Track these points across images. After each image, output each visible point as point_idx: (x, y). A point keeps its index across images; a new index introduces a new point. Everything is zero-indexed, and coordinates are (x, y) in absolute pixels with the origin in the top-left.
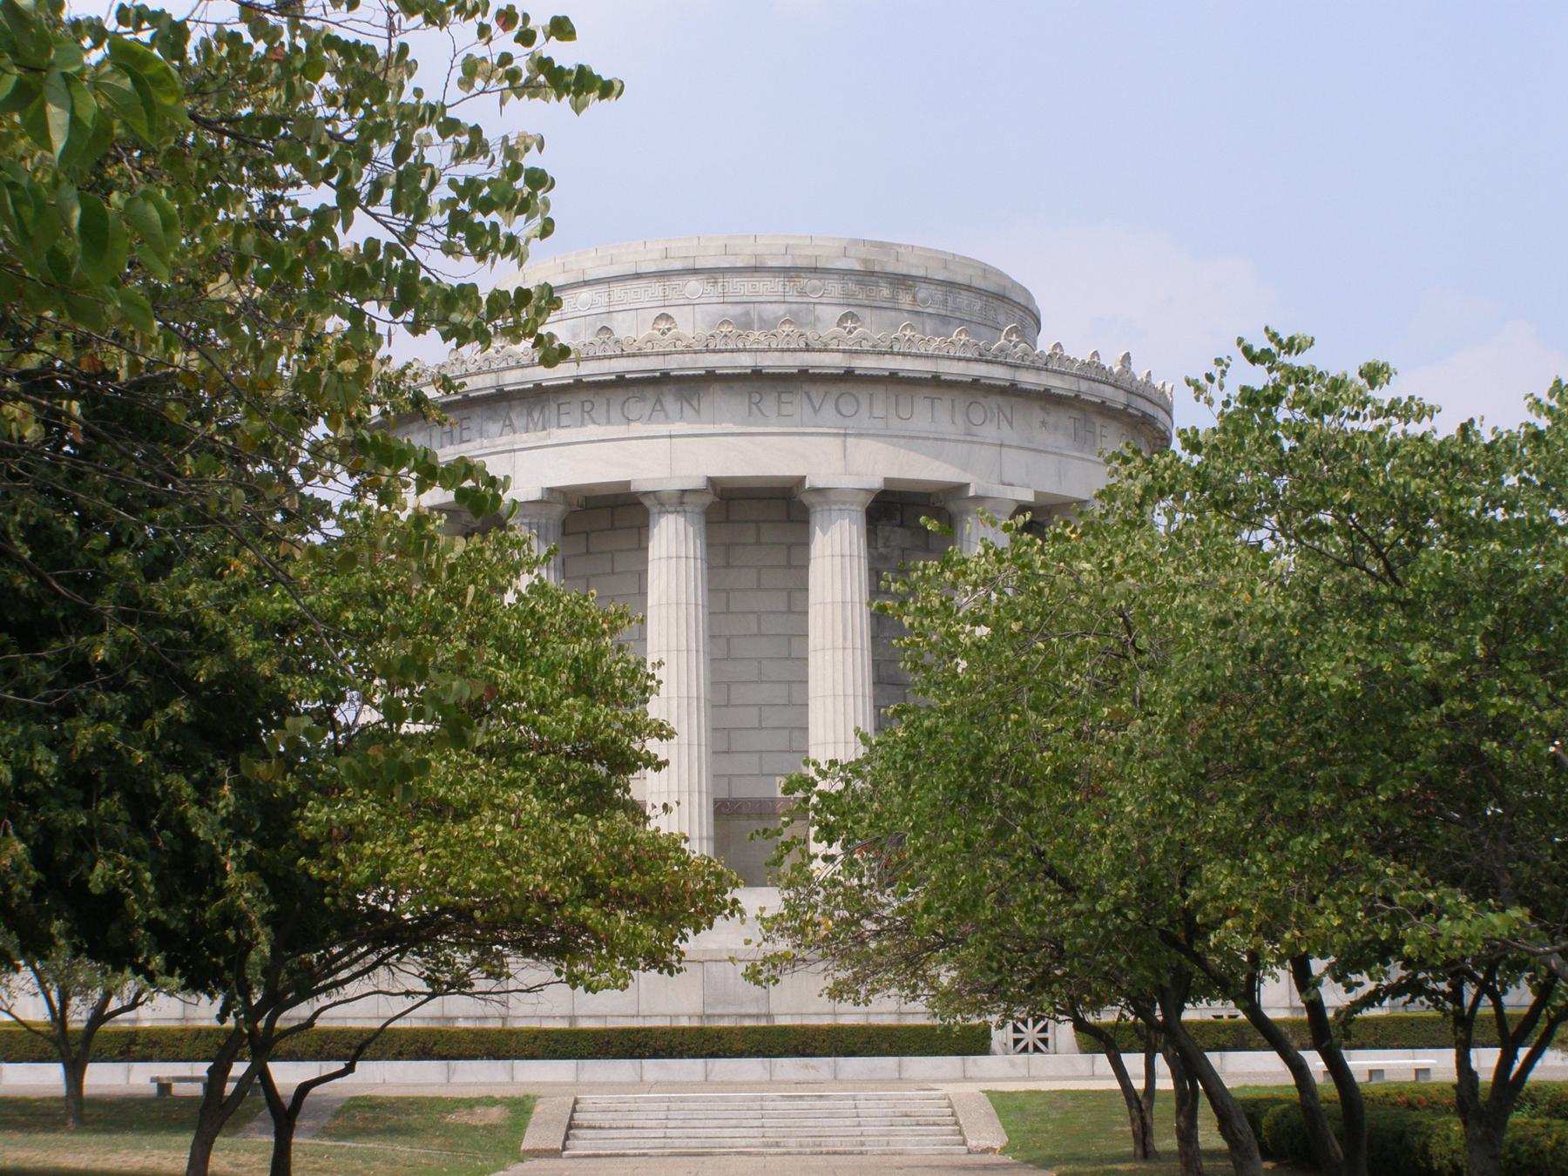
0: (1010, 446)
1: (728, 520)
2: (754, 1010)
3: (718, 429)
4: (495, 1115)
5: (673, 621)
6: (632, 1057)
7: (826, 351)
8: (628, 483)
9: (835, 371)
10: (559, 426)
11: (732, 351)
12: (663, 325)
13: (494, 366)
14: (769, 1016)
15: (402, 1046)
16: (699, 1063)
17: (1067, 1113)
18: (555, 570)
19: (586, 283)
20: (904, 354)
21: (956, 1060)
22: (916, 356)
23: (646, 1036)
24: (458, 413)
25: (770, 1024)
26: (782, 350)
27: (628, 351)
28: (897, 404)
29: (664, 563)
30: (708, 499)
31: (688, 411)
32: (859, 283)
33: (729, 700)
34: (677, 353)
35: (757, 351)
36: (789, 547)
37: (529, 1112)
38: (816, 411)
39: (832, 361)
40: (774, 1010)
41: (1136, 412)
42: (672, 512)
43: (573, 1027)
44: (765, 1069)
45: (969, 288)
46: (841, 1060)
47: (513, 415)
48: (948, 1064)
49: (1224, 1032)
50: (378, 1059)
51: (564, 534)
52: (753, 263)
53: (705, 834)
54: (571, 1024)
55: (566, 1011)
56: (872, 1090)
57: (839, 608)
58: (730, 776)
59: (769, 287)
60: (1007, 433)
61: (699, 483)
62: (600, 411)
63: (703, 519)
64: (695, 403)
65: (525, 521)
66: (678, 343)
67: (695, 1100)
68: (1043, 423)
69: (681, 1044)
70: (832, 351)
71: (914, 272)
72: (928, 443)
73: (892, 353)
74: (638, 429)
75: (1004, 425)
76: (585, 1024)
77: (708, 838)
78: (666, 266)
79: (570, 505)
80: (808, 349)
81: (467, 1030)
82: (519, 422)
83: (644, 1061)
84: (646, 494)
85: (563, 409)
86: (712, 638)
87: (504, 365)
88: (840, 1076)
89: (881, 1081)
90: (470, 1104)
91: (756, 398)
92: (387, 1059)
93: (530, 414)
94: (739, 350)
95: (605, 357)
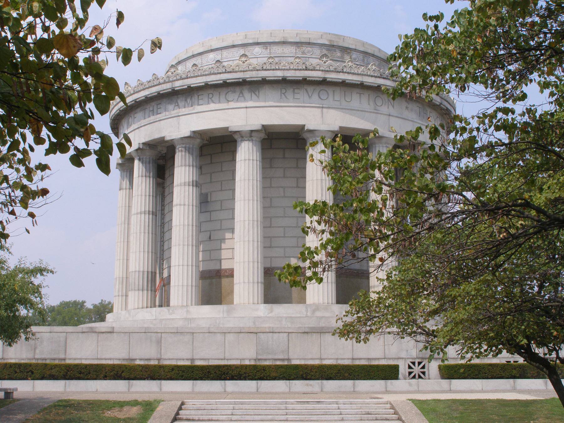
0: (392, 116)
1: (271, 148)
2: (281, 357)
3: (267, 104)
4: (134, 411)
5: (247, 187)
6: (221, 379)
7: (314, 70)
8: (228, 128)
9: (318, 79)
10: (198, 105)
11: (273, 70)
12: (243, 59)
13: (171, 79)
14: (289, 360)
15: (106, 373)
16: (254, 383)
17: (462, 413)
18: (196, 167)
19: (212, 51)
20: (348, 73)
21: (382, 382)
22: (353, 74)
23: (228, 369)
24: (156, 102)
25: (289, 364)
26: (295, 70)
27: (228, 70)
28: (345, 95)
29: (243, 162)
30: (263, 135)
31: (254, 96)
32: (328, 50)
33: (271, 224)
34: (249, 71)
35: (284, 70)
36: (298, 179)
37: (153, 410)
38: (310, 97)
39: (317, 75)
40: (291, 357)
41: (444, 107)
42: (246, 140)
43: (193, 364)
44: (287, 386)
45: (373, 55)
46: (325, 382)
47: (179, 101)
48: (378, 385)
49: (515, 369)
50: (95, 379)
51: (200, 156)
52: (282, 40)
53: (260, 281)
54: (191, 363)
55: (190, 357)
56: (346, 398)
57: (319, 182)
58: (271, 257)
59: (289, 50)
60: (392, 111)
61: (259, 127)
62: (216, 98)
63: (260, 144)
64: (257, 93)
65: (183, 146)
66: (250, 66)
67: (249, 403)
68: (407, 108)
69: (245, 373)
70: (317, 70)
71: (351, 47)
72: (358, 112)
73: (343, 72)
74: (232, 105)
75: (391, 107)
76: (198, 363)
77: (261, 283)
78: (246, 41)
79: (203, 140)
80: (307, 69)
81: (139, 365)
82: (181, 103)
83: (227, 381)
84: (235, 132)
85: (200, 97)
86: (264, 197)
87: (175, 79)
88: (324, 390)
89: (344, 393)
90: (121, 405)
91: (284, 91)
92: (100, 379)
93: (186, 100)
94: (276, 69)
95: (218, 73)
